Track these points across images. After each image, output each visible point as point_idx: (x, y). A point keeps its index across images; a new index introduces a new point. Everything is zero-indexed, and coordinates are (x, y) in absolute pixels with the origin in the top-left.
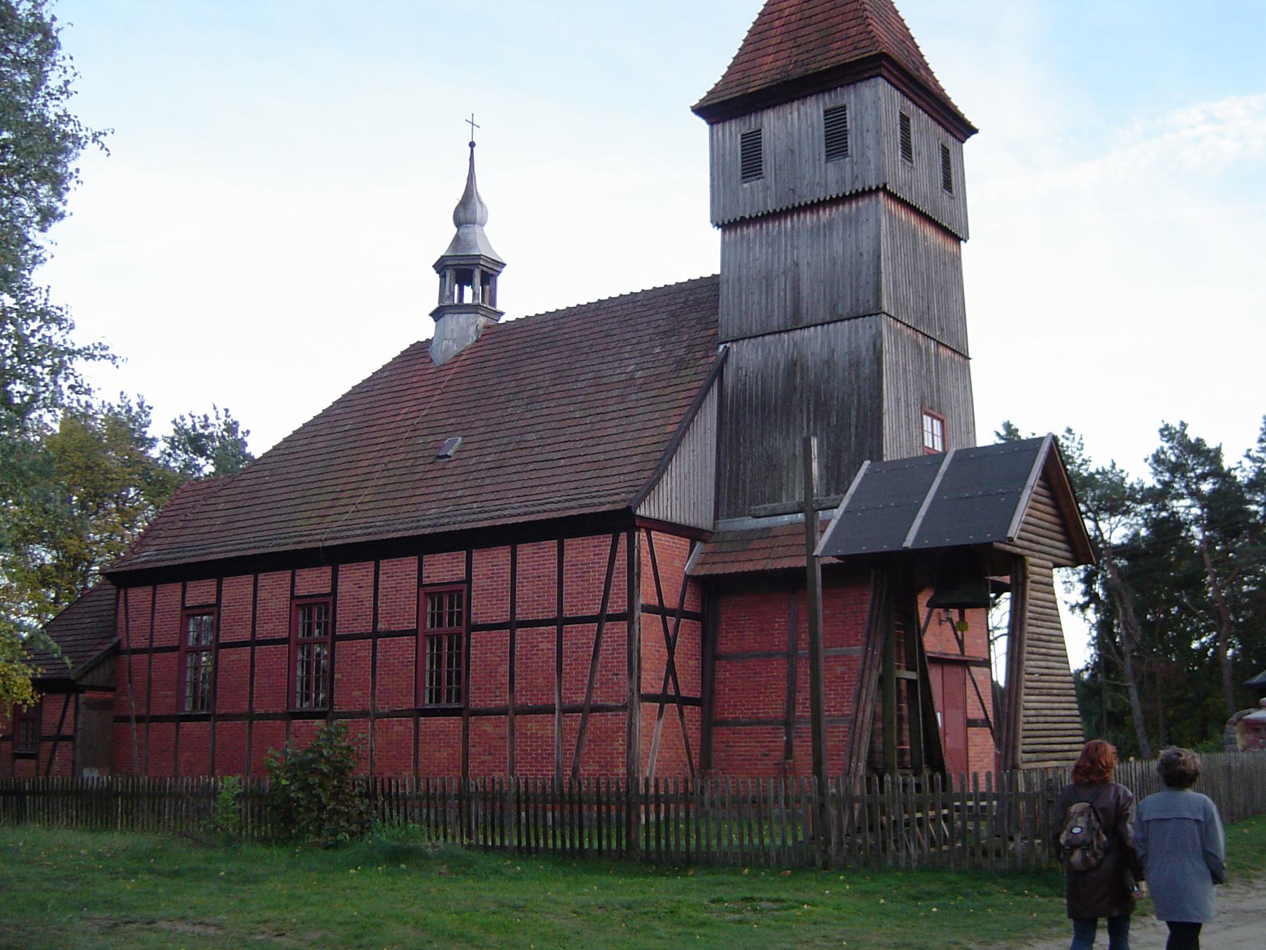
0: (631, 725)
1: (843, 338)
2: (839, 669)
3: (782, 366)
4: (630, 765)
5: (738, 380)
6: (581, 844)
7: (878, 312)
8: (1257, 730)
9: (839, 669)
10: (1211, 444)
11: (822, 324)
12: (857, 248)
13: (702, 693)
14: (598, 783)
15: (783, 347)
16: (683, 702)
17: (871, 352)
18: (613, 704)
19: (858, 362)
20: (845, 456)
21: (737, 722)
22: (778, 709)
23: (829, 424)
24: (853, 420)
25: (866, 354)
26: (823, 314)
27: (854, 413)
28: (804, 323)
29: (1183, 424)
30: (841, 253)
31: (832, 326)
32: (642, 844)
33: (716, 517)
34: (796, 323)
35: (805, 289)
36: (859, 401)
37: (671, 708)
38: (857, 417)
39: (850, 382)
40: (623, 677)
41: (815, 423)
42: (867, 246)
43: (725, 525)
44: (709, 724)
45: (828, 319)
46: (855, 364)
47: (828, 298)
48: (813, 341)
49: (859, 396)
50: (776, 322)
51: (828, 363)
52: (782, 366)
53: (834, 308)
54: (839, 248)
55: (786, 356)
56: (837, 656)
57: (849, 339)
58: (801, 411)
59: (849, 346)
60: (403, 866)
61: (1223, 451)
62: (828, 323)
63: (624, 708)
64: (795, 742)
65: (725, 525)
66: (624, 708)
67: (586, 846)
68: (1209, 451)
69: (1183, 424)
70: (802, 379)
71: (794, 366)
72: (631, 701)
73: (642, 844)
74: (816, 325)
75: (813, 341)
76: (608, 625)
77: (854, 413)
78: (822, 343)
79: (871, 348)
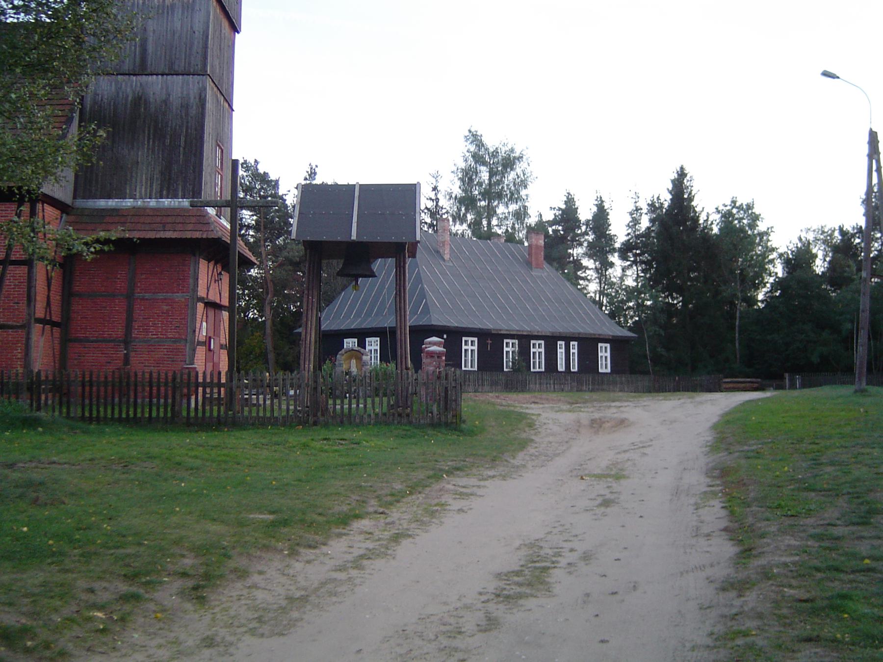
0: (28, 339)
1: (178, 87)
2: (165, 308)
3: (130, 98)
4: (27, 365)
5: (95, 102)
6: (135, 414)
7: (204, 73)
8: (432, 357)
9: (165, 308)
10: (273, 177)
11: (162, 75)
12: (192, 27)
13: (62, 318)
14: (166, 374)
15: (132, 86)
16: (54, 324)
17: (197, 100)
18: (15, 324)
19: (188, 105)
20: (175, 167)
21: (87, 340)
22: (120, 332)
23: (164, 143)
24: (182, 144)
25: (193, 101)
26: (162, 68)
27: (183, 139)
28: (149, 71)
29: (256, 161)
30: (179, 28)
31: (169, 77)
32: (184, 413)
33: (75, 197)
34: (142, 69)
35: (150, 48)
36: (187, 131)
37: (48, 327)
38: (185, 142)
39: (182, 118)
40: (23, 305)
41: (154, 142)
42: (198, 27)
43: (80, 203)
44: (66, 340)
45: (167, 72)
46: (185, 106)
47: (168, 58)
48: (155, 86)
49: (187, 127)
50: (126, 68)
51: (166, 102)
52: (130, 98)
53: (172, 64)
54: (178, 25)
55: (134, 92)
56: (165, 299)
57: (182, 88)
58: (144, 132)
59: (182, 93)
60: (40, 429)
61: (280, 183)
62: (167, 75)
63: (22, 327)
64: (132, 354)
65: (80, 203)
66: (22, 327)
67: (139, 415)
68: (272, 181)
69: (256, 161)
70: (145, 109)
71: (139, 100)
72: (29, 323)
73: (184, 413)
74: (157, 75)
75: (155, 86)
76: (11, 267)
77: (183, 139)
78: (162, 88)
79: (197, 97)
